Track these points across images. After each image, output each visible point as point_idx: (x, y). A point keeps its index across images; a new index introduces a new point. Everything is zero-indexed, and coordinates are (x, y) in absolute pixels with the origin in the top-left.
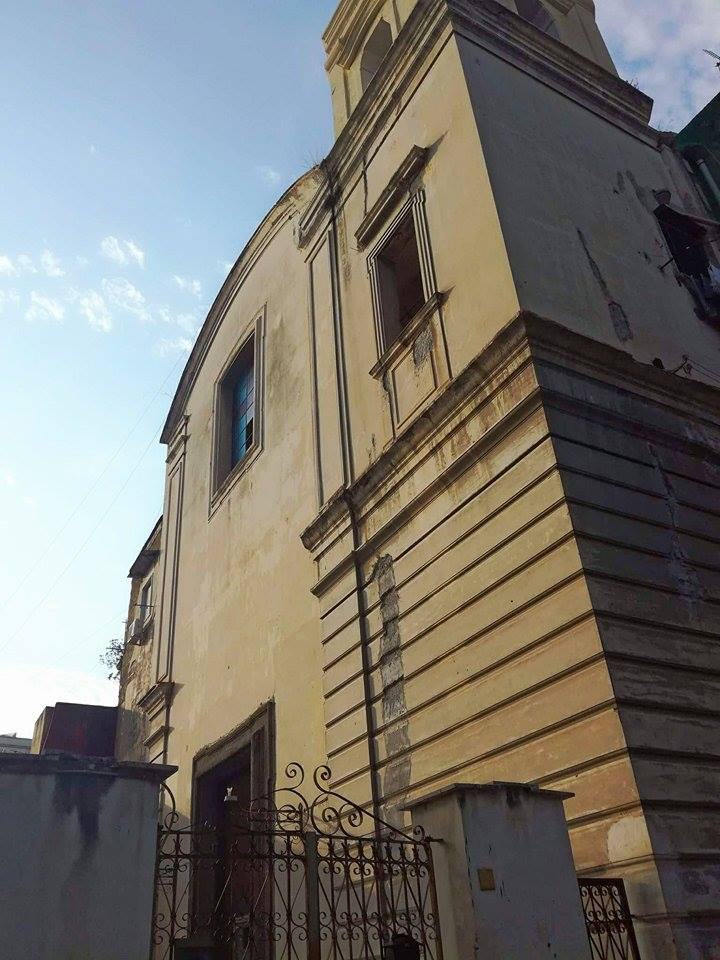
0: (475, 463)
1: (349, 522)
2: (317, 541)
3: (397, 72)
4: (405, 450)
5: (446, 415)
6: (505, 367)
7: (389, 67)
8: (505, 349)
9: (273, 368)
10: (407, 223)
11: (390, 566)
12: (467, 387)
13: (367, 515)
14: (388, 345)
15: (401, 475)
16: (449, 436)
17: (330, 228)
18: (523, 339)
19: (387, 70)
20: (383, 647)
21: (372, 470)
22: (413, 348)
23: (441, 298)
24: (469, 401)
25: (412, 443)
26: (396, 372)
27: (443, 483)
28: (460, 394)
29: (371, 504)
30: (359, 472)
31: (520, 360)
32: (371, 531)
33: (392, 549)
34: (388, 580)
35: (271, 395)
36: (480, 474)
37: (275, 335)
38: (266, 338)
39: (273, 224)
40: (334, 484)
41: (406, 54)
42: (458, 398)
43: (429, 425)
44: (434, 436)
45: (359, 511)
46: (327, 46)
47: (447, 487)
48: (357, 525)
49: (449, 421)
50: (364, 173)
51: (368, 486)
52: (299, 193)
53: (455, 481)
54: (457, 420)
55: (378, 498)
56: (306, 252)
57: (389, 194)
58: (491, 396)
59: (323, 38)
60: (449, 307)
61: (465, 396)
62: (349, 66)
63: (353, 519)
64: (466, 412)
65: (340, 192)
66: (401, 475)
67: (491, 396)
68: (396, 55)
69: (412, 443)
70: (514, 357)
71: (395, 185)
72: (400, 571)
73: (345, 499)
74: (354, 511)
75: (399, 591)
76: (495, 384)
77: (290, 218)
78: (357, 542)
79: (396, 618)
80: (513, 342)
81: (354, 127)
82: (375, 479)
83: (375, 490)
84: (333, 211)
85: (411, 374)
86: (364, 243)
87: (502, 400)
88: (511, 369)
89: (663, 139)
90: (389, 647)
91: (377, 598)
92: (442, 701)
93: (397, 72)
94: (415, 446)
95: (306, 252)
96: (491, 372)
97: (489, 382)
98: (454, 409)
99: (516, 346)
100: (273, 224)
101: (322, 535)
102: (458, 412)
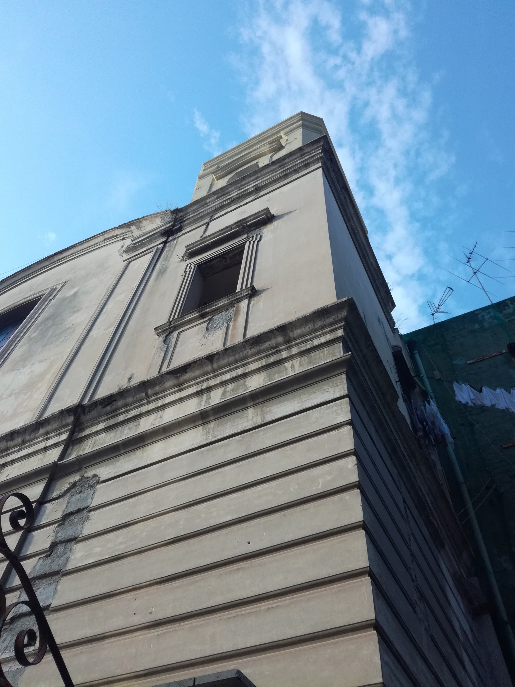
0: (247, 408)
1: (64, 437)
2: (15, 446)
3: (263, 180)
4: (168, 384)
5: (229, 364)
6: (311, 339)
7: (259, 175)
8: (319, 324)
9: (47, 319)
10: (240, 250)
11: (92, 487)
12: (267, 345)
13: (88, 437)
14: (186, 310)
15: (152, 406)
16: (223, 383)
17: (160, 246)
18: (340, 321)
19: (256, 176)
20: (38, 568)
21: (122, 394)
22: (210, 320)
23: (253, 293)
24: (260, 359)
25: (181, 380)
26: (183, 334)
27: (202, 418)
28: (254, 350)
29: (101, 426)
30: (102, 393)
31: (329, 337)
32: (88, 448)
33: (104, 471)
34: (85, 499)
35: (34, 335)
36: (251, 416)
37: (64, 299)
38: (53, 302)
39: (106, 239)
40: (69, 397)
41: (276, 172)
42: (250, 352)
43: (209, 368)
44: (208, 379)
45: (82, 430)
46: (202, 172)
47: (204, 424)
48: (71, 442)
49: (231, 370)
50: (208, 224)
51: (108, 408)
52: (142, 225)
53: (215, 419)
54: (240, 371)
55: (112, 422)
56: (126, 256)
57: (230, 230)
58: (286, 360)
59: (204, 164)
60: (258, 302)
61: (259, 353)
62: (218, 179)
63: (72, 433)
64: (253, 366)
65: (180, 229)
66: (152, 406)
67: (286, 360)
68: (268, 170)
69: (181, 380)
70: (324, 334)
71: (238, 226)
72: (102, 494)
73: (75, 415)
74: (78, 426)
75: (92, 513)
76: (295, 350)
77: (123, 239)
78: (62, 456)
79: (74, 540)
80: (331, 319)
81: (212, 198)
82: (120, 403)
83: (114, 413)
84: (167, 239)
85: (200, 337)
86: (191, 254)
87: (298, 362)
88: (316, 342)
89: (401, 336)
90: (47, 569)
91: (59, 515)
92: (95, 645)
93: (263, 180)
94: (182, 384)
95: (126, 256)
96: (295, 339)
97: (289, 348)
98: (243, 361)
99: (331, 324)
100: (106, 239)
101: (24, 442)
102: (244, 365)
